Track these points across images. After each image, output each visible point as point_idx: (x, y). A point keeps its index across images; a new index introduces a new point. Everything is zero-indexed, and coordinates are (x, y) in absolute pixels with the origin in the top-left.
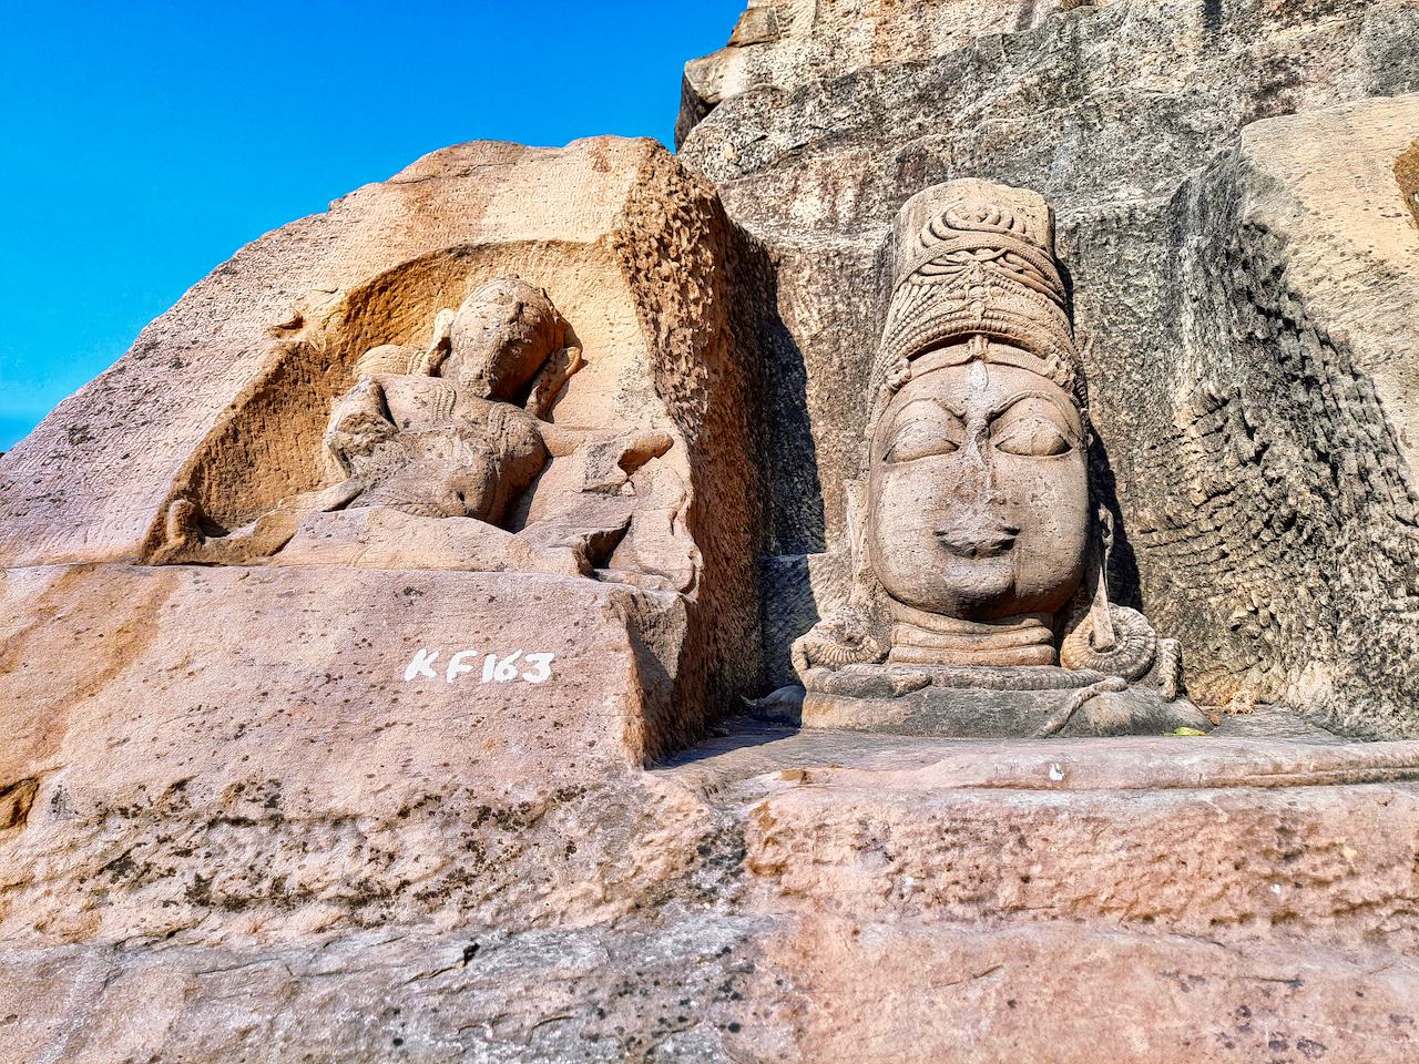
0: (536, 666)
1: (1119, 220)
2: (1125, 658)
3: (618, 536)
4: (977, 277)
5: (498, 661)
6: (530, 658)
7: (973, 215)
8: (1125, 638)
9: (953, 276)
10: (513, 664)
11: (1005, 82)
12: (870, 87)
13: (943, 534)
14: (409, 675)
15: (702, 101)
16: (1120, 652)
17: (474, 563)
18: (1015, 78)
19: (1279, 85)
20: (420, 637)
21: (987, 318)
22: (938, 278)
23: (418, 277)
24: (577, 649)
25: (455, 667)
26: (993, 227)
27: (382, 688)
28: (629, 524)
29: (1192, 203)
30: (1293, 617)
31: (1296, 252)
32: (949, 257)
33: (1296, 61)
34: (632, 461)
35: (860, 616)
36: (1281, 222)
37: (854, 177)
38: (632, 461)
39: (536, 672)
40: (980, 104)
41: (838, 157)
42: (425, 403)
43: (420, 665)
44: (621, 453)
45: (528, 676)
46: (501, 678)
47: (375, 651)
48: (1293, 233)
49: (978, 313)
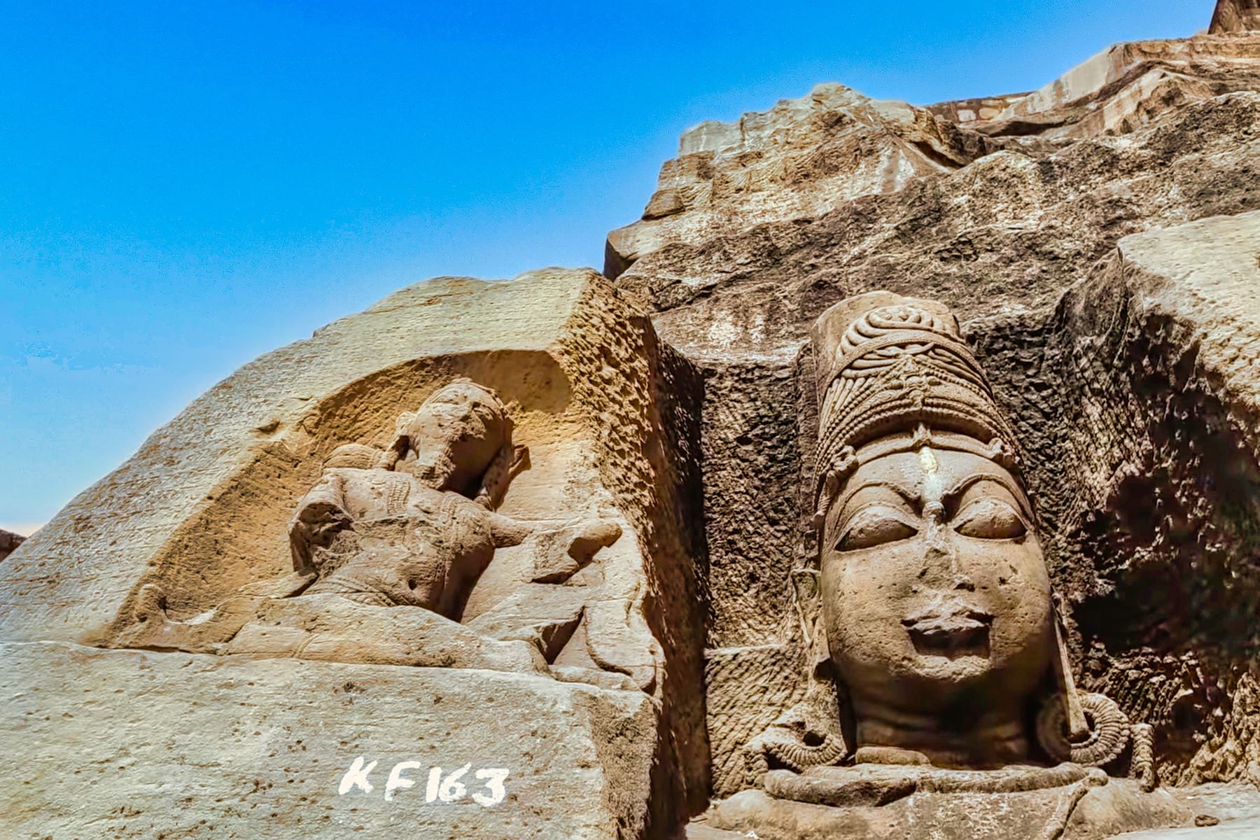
0: (488, 785)
1: (1012, 328)
2: (1100, 747)
3: (568, 630)
4: (911, 367)
5: (444, 775)
6: (481, 774)
7: (895, 316)
8: (1099, 726)
9: (887, 368)
10: (460, 780)
11: (881, 230)
12: (767, 239)
13: (913, 622)
14: (344, 789)
15: (623, 259)
16: (1096, 740)
17: (419, 656)
18: (887, 227)
19: (1120, 218)
20: (357, 742)
21: (928, 405)
22: (872, 371)
23: (383, 385)
24: (537, 763)
25: (395, 781)
26: (916, 325)
27: (313, 802)
28: (581, 615)
29: (1079, 309)
30: (1247, 691)
31: (1205, 335)
32: (880, 352)
33: (1130, 201)
34: (584, 551)
35: (820, 713)
36: (1184, 311)
37: (762, 305)
38: (584, 551)
39: (488, 793)
40: (863, 246)
41: (743, 289)
42: (380, 494)
43: (356, 776)
44: (570, 541)
45: (477, 797)
46: (446, 797)
47: (309, 755)
48: (1198, 319)
49: (919, 400)
